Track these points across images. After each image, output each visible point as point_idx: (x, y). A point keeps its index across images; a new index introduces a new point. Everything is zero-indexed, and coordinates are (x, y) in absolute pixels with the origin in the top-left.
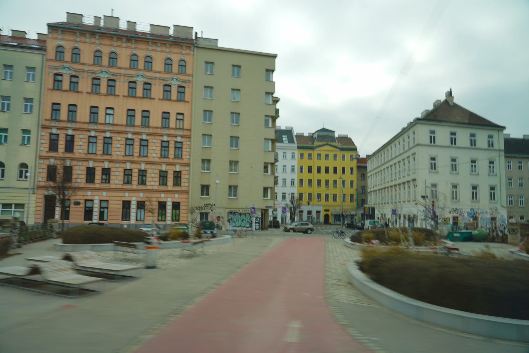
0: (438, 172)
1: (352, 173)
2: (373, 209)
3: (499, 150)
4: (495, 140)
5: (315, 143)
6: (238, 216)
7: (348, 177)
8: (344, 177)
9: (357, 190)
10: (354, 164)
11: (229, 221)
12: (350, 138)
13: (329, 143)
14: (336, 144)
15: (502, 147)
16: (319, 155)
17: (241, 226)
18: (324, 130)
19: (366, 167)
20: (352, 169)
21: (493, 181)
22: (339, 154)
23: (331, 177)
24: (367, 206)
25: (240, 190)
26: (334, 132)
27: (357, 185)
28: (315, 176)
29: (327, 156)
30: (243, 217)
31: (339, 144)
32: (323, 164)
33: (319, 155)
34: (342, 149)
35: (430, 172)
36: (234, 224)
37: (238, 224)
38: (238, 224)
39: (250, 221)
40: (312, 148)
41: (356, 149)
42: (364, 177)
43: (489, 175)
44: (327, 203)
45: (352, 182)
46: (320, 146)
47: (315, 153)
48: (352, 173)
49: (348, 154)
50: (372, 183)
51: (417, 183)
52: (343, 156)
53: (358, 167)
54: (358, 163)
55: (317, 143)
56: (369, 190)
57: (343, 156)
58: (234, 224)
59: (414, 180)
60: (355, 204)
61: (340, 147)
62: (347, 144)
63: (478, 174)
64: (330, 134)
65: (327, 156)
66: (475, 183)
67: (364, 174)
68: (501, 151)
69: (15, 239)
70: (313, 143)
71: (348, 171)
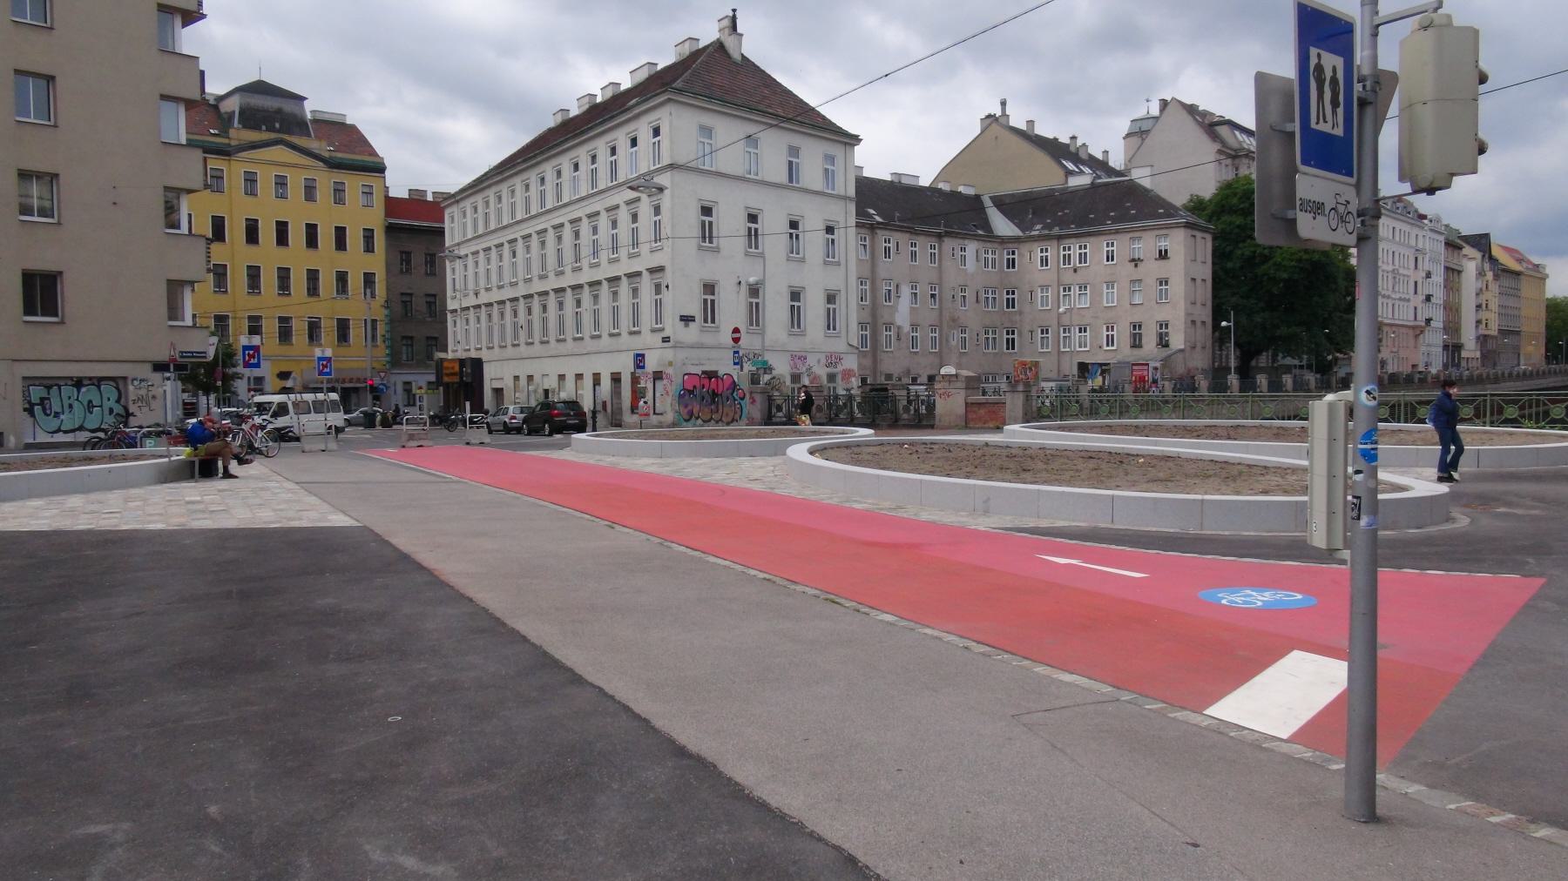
0: (717, 250)
1: (369, 248)
2: (477, 364)
3: (845, 198)
4: (839, 167)
5: (232, 133)
6: (67, 391)
7: (356, 262)
8: (344, 261)
9: (387, 305)
10: (376, 219)
11: (30, 411)
12: (353, 130)
13: (286, 137)
14: (313, 145)
15: (852, 192)
16: (251, 179)
17: (81, 428)
18: (260, 88)
19: (441, 232)
20: (369, 235)
21: (834, 280)
22: (326, 180)
23: (297, 257)
24: (450, 356)
25: (71, 294)
26: (303, 99)
27: (388, 289)
28: (268, 255)
29: (281, 182)
30: (88, 393)
31: (324, 144)
32: (267, 213)
33: (251, 179)
34: (334, 165)
35: (700, 248)
36: (55, 424)
37: (67, 420)
38: (67, 420)
39: (118, 409)
40: (224, 152)
41: (380, 169)
42: (432, 263)
43: (826, 263)
44: (285, 349)
45: (369, 279)
46: (254, 146)
47: (234, 171)
48: (369, 248)
49: (354, 183)
50: (463, 283)
51: (668, 277)
52: (339, 191)
53: (391, 230)
54: (388, 213)
55: (239, 134)
56: (451, 305)
57: (339, 191)
58: (55, 424)
59: (657, 270)
60: (382, 352)
61: (327, 155)
62: (350, 154)
63: (803, 260)
64: (288, 107)
65: (281, 182)
66: (797, 282)
67: (433, 256)
68: (850, 199)
69: (1230, 265)
70: (224, 132)
71: (354, 239)
